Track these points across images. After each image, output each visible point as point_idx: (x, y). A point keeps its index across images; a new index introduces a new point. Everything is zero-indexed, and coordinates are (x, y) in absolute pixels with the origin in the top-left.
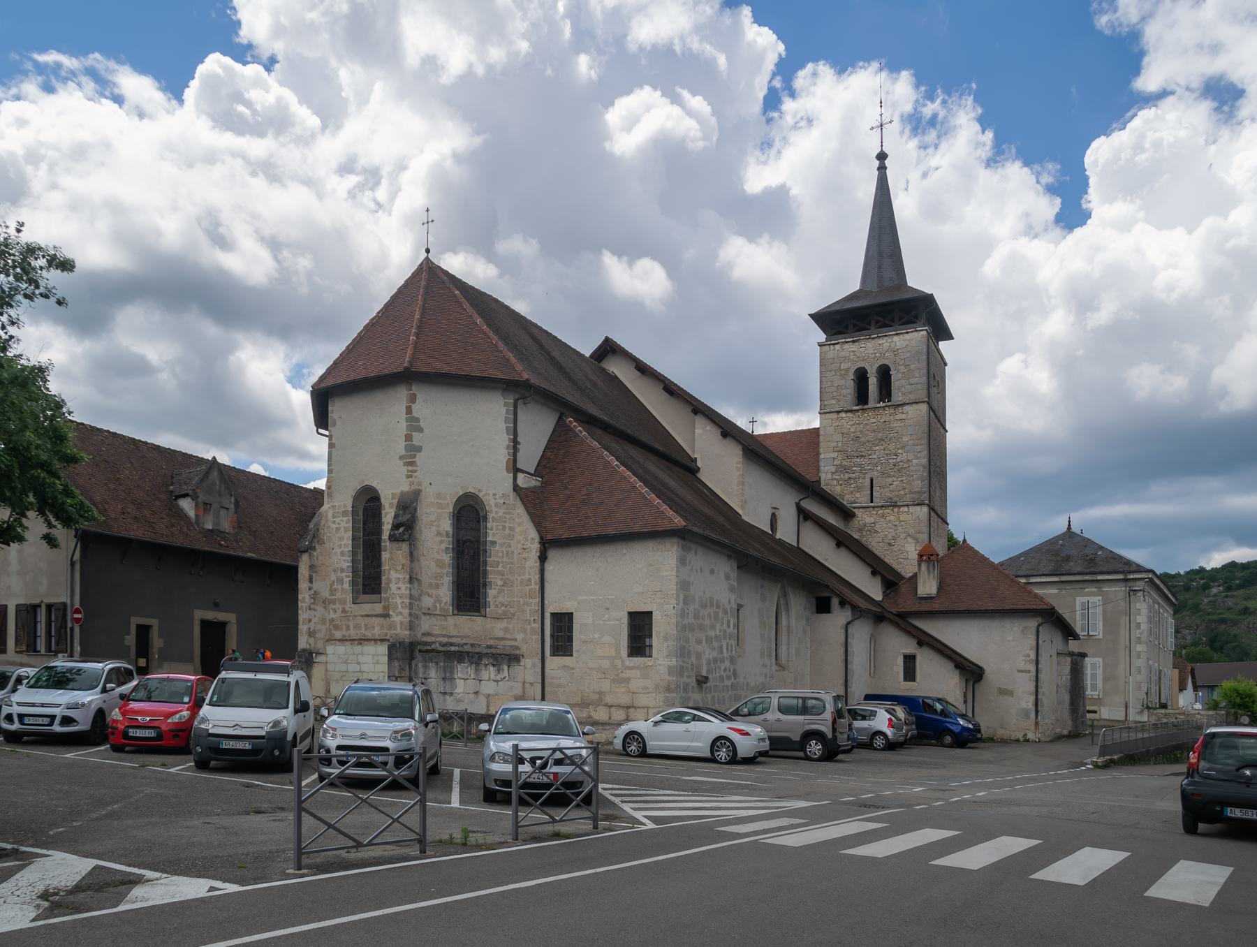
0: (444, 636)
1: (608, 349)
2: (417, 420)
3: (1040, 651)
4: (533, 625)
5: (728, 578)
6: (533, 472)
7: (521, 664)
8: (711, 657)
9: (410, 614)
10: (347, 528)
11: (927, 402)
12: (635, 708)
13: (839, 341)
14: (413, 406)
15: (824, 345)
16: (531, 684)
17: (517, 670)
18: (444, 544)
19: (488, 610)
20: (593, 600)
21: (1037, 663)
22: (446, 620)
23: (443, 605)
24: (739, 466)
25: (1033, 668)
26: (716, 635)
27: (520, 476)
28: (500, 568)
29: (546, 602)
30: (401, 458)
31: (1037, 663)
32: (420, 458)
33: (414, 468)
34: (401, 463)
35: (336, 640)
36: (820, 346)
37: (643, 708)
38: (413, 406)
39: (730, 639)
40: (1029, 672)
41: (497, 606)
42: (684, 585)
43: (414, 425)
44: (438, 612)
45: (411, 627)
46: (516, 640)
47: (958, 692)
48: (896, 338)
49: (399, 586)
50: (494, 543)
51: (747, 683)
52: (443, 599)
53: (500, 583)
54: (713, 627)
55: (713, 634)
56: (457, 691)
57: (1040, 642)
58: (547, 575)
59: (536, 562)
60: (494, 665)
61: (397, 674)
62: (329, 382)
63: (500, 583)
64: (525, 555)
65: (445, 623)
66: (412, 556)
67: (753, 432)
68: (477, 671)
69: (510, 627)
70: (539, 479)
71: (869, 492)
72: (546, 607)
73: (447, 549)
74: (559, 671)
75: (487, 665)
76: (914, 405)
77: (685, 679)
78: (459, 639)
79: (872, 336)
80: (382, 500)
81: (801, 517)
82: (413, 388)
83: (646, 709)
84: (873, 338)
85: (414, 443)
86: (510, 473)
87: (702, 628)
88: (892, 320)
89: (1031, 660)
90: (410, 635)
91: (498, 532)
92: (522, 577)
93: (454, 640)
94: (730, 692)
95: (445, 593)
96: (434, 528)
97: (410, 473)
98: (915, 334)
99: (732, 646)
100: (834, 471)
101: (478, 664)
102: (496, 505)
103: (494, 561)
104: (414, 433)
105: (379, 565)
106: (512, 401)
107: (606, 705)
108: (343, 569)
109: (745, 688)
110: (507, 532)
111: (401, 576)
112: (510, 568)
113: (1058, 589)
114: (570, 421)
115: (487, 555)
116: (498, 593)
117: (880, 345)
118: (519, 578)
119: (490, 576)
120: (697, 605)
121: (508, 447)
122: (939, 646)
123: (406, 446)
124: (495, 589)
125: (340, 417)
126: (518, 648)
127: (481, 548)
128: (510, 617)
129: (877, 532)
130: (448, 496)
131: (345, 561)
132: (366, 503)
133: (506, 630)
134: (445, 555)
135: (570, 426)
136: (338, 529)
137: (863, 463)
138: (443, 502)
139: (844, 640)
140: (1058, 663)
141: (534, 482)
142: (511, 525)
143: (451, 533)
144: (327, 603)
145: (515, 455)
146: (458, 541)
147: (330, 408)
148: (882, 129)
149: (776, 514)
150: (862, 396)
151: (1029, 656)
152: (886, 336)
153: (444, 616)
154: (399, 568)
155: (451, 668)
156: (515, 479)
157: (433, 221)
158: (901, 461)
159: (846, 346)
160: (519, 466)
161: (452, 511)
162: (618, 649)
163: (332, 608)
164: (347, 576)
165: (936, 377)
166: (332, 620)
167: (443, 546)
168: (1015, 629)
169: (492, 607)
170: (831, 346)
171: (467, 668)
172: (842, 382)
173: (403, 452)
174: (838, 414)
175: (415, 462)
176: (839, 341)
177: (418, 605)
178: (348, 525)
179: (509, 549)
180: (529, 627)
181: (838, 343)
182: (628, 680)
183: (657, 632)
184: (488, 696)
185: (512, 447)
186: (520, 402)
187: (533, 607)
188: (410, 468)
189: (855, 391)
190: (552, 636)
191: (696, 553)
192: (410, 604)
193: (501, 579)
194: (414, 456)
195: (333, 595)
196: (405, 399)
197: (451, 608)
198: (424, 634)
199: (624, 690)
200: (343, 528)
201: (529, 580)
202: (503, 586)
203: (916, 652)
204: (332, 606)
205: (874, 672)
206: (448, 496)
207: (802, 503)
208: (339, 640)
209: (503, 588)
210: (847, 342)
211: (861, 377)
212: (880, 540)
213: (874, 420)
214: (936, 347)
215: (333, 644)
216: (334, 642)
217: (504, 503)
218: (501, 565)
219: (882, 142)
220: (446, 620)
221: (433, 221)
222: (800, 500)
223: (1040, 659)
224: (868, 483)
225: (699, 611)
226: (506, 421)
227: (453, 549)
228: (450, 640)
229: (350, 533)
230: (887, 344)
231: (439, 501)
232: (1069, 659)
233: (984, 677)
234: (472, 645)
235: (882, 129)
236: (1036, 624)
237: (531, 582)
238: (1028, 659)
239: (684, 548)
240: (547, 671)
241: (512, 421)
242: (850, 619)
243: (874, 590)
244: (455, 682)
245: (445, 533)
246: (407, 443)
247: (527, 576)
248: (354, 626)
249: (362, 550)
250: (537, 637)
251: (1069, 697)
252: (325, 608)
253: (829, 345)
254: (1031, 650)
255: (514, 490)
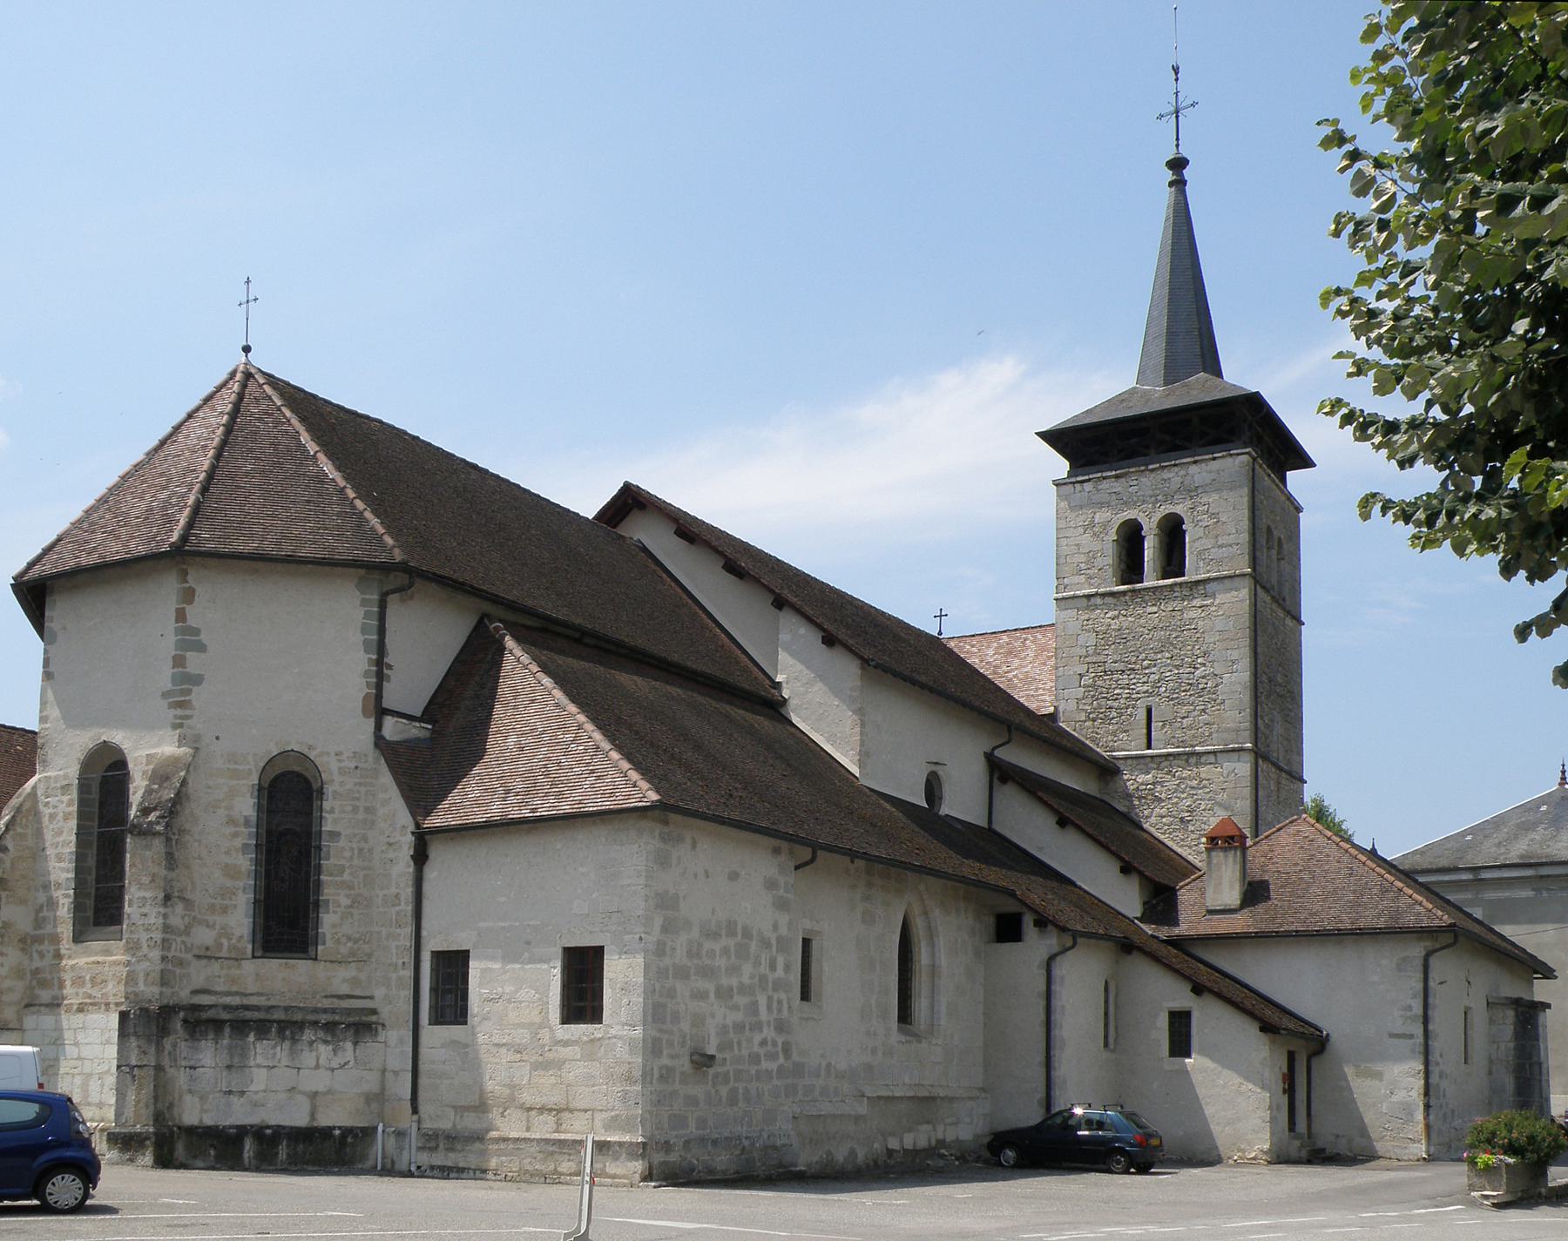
0: (237, 993)
1: (630, 502)
2: (196, 632)
3: (1431, 1000)
4: (402, 973)
5: (771, 885)
6: (419, 715)
7: (380, 1039)
8: (729, 1021)
9: (164, 958)
10: (70, 814)
11: (1250, 575)
12: (571, 1111)
13: (1091, 476)
14: (188, 609)
15: (1065, 484)
16: (396, 1073)
17: (370, 1048)
18: (240, 839)
19: (320, 948)
20: (504, 928)
21: (1426, 1020)
22: (239, 967)
23: (234, 941)
24: (855, 694)
25: (1418, 1030)
26: (741, 982)
27: (389, 722)
28: (346, 876)
29: (424, 933)
30: (165, 695)
31: (1426, 1020)
32: (199, 696)
33: (188, 712)
34: (165, 703)
35: (41, 1005)
36: (1056, 485)
37: (586, 1111)
38: (188, 609)
39: (775, 989)
40: (1411, 1036)
41: (338, 941)
42: (665, 902)
43: (190, 641)
44: (224, 953)
45: (165, 980)
46: (371, 998)
47: (1267, 1074)
48: (1193, 469)
49: (144, 910)
50: (335, 835)
51: (829, 1065)
52: (234, 931)
53: (345, 901)
54: (734, 970)
55: (734, 982)
56: (252, 1088)
57: (1431, 984)
58: (427, 888)
59: (409, 866)
60: (326, 1042)
61: (134, 1062)
62: (47, 568)
63: (345, 901)
64: (391, 855)
65: (238, 972)
66: (171, 861)
67: (940, 633)
68: (293, 1053)
69: (363, 976)
70: (426, 725)
71: (1145, 731)
72: (424, 941)
73: (245, 846)
74: (443, 1050)
75: (311, 1043)
76: (1226, 581)
77: (665, 1061)
78: (263, 998)
79: (1151, 467)
80: (131, 766)
81: (996, 776)
82: (189, 578)
83: (590, 1113)
84: (587, 645)
85: (188, 670)
86: (368, 717)
87: (708, 972)
88: (1147, 447)
89: (1416, 1016)
90: (161, 993)
91: (343, 816)
92: (386, 892)
93: (254, 1001)
94: (775, 1082)
95: (240, 920)
96: (222, 812)
97: (178, 721)
98: (1230, 460)
99: (780, 1002)
100: (1080, 696)
101: (294, 1041)
102: (342, 771)
103: (336, 865)
104: (188, 654)
105: (121, 875)
106: (376, 597)
107: (522, 1107)
108: (59, 884)
109: (823, 1073)
110: (361, 816)
111: (148, 894)
112: (365, 876)
113: (1533, 890)
114: (497, 629)
115: (322, 855)
116: (342, 919)
117: (1165, 480)
118: (381, 894)
119: (326, 891)
120: (695, 933)
121: (366, 674)
122: (1237, 994)
123: (173, 674)
124: (335, 912)
125: (65, 629)
126: (374, 1012)
127: (313, 844)
128: (362, 960)
129: (1160, 800)
130: (250, 758)
131: (62, 869)
132: (105, 772)
133: (355, 981)
134: (240, 856)
135: (493, 636)
136: (52, 817)
137: (1134, 681)
138: (241, 768)
139: (1044, 988)
140: (1491, 1021)
141: (417, 731)
142: (368, 804)
143: (254, 820)
144: (29, 941)
145: (379, 687)
146: (269, 832)
147: (47, 613)
148: (1177, 117)
149: (941, 773)
150: (1131, 567)
151: (1410, 1008)
152: (1175, 465)
153: (237, 960)
154: (146, 880)
155: (243, 1049)
156: (379, 726)
157: (256, 299)
158: (1203, 677)
159: (1104, 485)
160: (385, 705)
161: (256, 782)
162: (544, 1011)
163: (37, 951)
164: (67, 896)
165: (1276, 533)
166: (37, 971)
167: (238, 843)
168: (1384, 962)
169: (329, 943)
170: (1078, 486)
171: (274, 1047)
172: (1096, 546)
173: (170, 686)
174: (1089, 600)
175: (190, 700)
176: (1091, 476)
177: (183, 942)
178: (71, 809)
179: (363, 845)
180: (394, 976)
181: (1089, 480)
182: (559, 1064)
183: (611, 980)
184: (314, 1096)
185: (374, 674)
186: (393, 600)
187: (402, 942)
188: (179, 712)
189: (1121, 560)
190: (434, 990)
191: (694, 847)
192: (164, 940)
193: (347, 896)
194: (189, 692)
195: (40, 928)
196: (174, 598)
197: (250, 947)
198: (195, 992)
199: (553, 1080)
200: (61, 814)
201: (397, 896)
202: (351, 906)
203: (1191, 1005)
204: (36, 947)
205: (1116, 1040)
206: (250, 758)
207: (996, 753)
208: (47, 1005)
209: (351, 910)
210: (1104, 478)
211: (1131, 537)
212: (1164, 811)
213: (1155, 609)
214: (1282, 492)
215: (34, 1013)
216: (37, 1008)
217: (356, 767)
218: (347, 871)
219: (1178, 139)
220: (239, 967)
221: (256, 299)
222: (994, 749)
223: (1430, 1013)
224: (1141, 715)
225: (700, 945)
226: (364, 630)
227: (256, 846)
228: (246, 1001)
229: (73, 823)
230: (1179, 479)
231: (231, 767)
232: (1511, 1013)
233: (1329, 1047)
234: (286, 1009)
235: (1177, 117)
236: (1423, 953)
237: (399, 899)
238: (1409, 1014)
239: (664, 838)
240: (424, 1051)
241: (375, 630)
242: (1056, 949)
243: (1126, 899)
244: (64, 1049)
245: (242, 821)
246: (176, 670)
247: (393, 890)
248: (708, 997)
249: (95, 852)
250: (407, 992)
251: (1512, 1080)
252: (23, 950)
253: (1074, 483)
254: (1414, 997)
255: (376, 745)
